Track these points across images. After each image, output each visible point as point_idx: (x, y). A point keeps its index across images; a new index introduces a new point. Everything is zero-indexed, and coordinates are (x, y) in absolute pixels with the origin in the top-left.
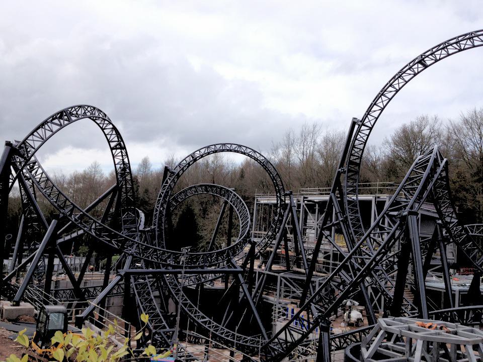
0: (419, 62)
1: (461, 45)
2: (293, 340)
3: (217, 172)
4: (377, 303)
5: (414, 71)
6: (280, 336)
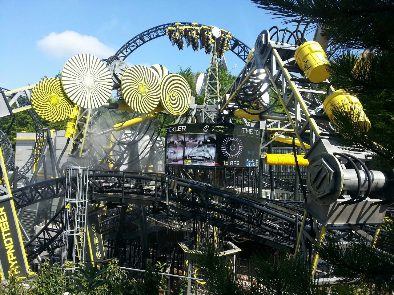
0: (140, 38)
1: (137, 43)
2: (51, 238)
3: (344, 89)
4: (194, 278)
5: (137, 44)
6: (40, 236)
